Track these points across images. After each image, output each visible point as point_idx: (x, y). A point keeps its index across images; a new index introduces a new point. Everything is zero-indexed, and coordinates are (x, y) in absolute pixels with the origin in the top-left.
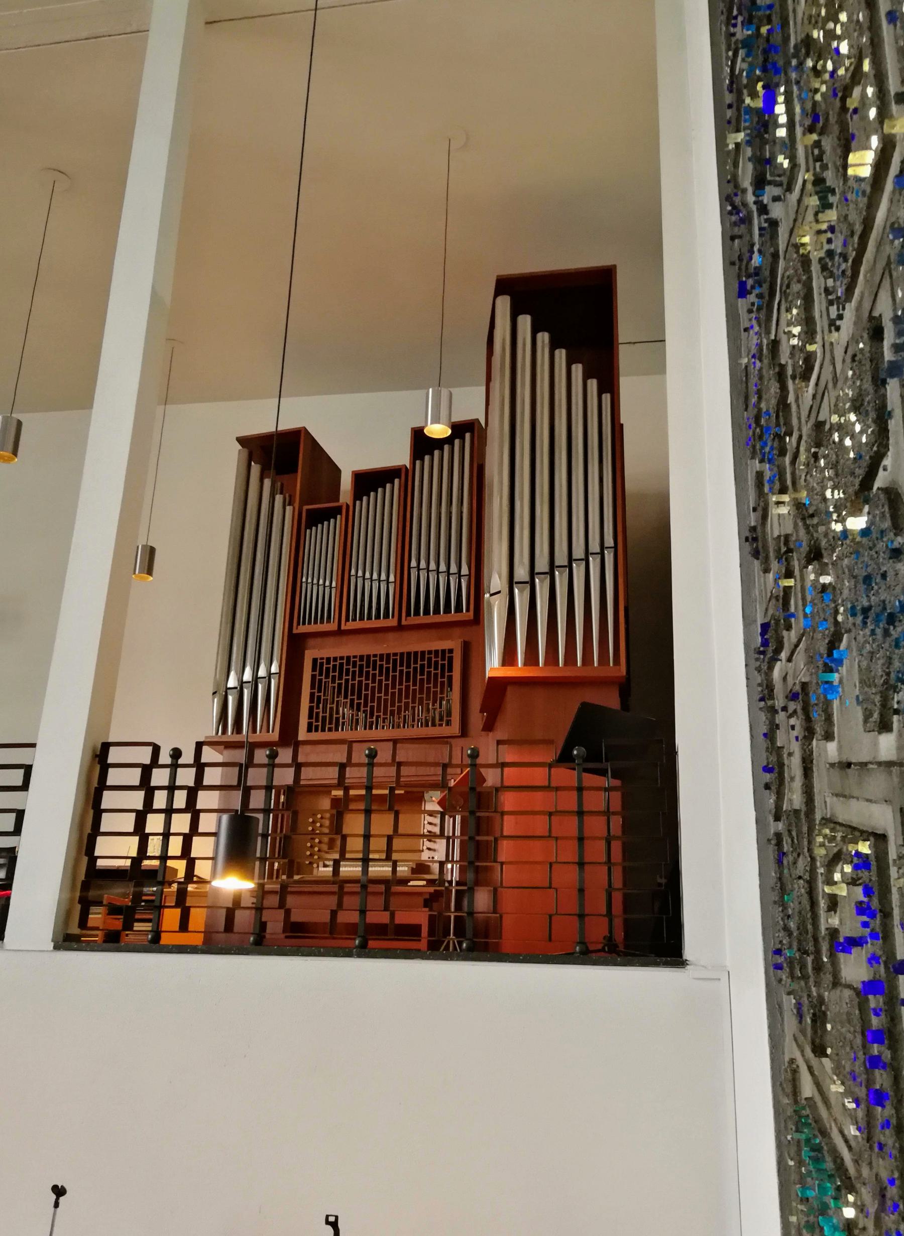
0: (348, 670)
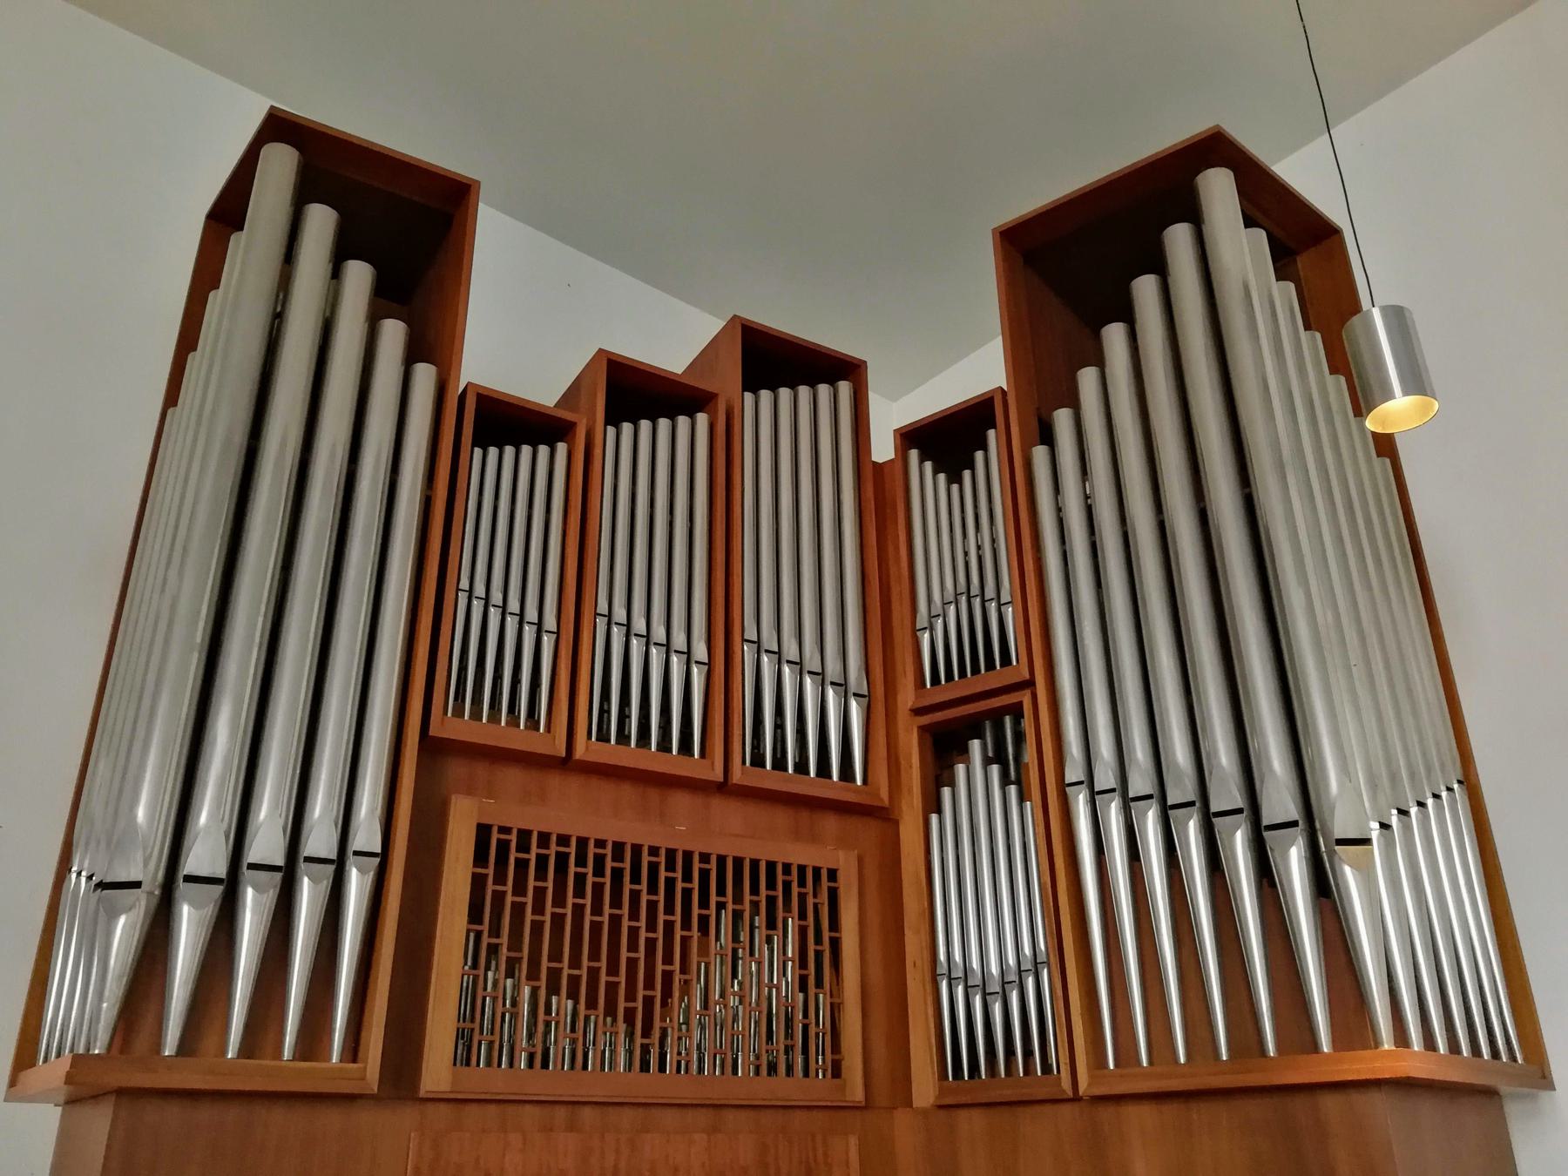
0: (580, 879)
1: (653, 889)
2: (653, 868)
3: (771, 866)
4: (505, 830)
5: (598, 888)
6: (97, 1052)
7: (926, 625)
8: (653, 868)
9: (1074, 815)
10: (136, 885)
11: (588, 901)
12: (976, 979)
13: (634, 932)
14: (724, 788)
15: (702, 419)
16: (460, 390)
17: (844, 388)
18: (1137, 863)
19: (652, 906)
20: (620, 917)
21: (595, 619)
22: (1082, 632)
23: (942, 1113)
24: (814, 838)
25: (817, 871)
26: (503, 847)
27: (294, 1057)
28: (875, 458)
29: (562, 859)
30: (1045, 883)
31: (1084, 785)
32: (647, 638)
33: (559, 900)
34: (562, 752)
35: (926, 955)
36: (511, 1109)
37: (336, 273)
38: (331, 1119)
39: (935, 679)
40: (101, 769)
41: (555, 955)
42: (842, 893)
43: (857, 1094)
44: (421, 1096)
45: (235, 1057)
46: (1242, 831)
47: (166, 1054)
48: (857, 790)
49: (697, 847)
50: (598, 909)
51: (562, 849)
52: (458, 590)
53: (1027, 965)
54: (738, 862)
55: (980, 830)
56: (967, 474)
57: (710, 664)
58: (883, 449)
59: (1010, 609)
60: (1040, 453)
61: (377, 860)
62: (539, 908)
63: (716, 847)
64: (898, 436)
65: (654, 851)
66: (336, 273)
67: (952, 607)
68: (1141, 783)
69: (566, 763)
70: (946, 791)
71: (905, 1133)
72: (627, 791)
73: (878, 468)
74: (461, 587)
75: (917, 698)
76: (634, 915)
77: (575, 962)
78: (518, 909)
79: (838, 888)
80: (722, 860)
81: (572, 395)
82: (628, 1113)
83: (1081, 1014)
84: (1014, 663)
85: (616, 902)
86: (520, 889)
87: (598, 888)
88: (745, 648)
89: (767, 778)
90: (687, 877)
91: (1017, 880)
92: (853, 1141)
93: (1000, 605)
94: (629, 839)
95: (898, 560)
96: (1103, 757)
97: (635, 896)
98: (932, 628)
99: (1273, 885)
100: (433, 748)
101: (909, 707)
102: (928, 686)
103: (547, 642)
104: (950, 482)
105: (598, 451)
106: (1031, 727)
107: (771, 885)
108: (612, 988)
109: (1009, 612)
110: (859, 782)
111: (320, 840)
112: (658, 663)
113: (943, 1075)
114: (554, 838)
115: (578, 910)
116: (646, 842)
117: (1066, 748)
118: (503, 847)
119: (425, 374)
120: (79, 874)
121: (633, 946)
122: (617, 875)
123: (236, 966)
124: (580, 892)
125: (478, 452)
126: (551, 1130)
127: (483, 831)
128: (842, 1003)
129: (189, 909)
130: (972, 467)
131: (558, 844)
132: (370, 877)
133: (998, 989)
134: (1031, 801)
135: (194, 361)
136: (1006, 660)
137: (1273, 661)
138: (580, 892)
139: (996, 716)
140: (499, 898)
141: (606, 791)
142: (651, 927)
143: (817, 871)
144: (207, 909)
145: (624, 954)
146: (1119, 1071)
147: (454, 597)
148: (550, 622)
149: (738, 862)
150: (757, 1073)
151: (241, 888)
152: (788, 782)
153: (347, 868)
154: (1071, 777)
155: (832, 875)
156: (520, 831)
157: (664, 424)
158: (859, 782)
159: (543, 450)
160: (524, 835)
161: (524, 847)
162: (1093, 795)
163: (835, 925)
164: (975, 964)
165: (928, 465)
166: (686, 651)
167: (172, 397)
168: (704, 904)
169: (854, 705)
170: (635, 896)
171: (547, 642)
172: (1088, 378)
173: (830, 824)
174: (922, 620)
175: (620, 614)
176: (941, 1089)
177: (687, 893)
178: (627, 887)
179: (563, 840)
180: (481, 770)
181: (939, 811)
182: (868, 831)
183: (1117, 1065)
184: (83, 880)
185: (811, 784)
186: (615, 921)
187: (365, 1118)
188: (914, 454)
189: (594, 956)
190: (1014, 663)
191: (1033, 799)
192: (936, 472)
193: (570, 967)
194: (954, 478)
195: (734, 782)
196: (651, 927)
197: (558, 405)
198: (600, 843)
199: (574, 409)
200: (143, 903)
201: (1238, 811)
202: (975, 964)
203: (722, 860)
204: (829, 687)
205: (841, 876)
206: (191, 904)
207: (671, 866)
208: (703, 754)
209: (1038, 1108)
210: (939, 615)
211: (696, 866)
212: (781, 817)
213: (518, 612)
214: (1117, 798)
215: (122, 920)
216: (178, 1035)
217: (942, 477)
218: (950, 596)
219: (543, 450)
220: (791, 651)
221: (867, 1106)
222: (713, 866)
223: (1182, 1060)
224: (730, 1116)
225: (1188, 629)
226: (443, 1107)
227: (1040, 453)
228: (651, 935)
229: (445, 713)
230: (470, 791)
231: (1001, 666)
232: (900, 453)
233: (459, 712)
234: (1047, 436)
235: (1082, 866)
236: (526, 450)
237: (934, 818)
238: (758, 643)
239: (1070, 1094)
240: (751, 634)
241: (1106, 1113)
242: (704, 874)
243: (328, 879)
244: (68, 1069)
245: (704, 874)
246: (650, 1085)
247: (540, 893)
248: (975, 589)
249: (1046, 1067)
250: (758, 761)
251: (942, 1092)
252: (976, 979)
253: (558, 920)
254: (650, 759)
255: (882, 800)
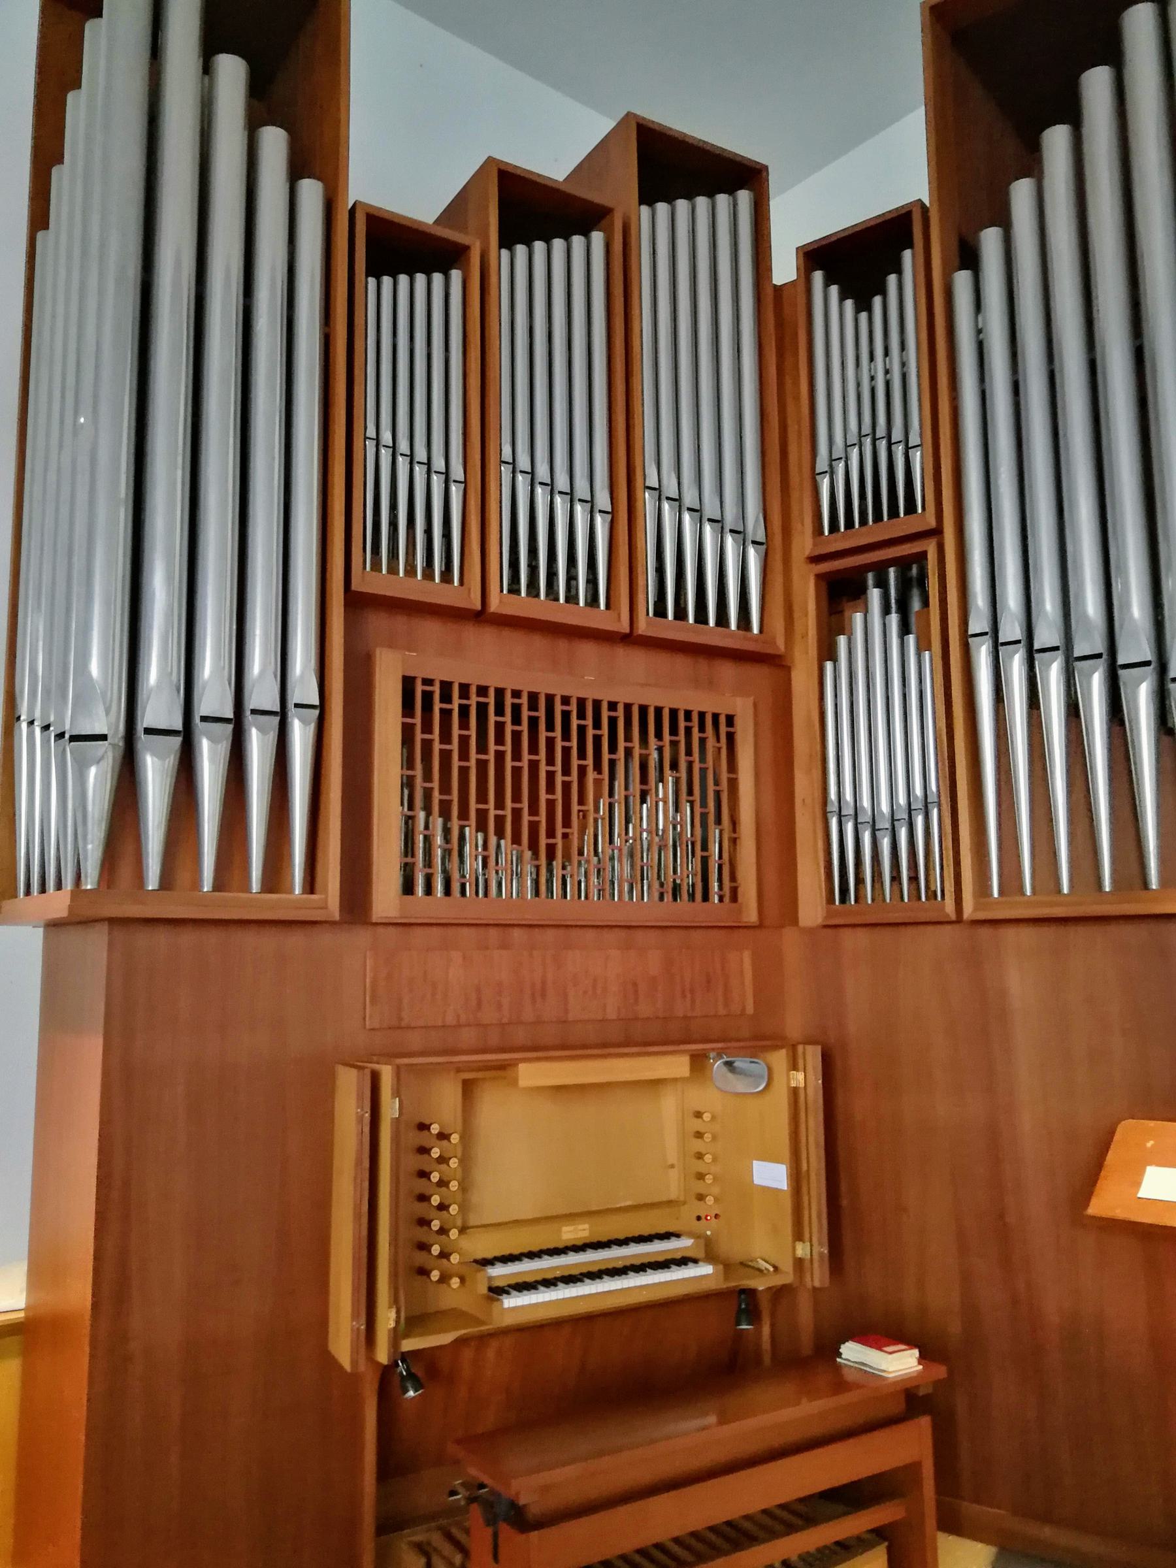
1: (566, 736)
2: (566, 715)
3: (674, 713)
4: (428, 682)
5: (516, 736)
6: (89, 887)
7: (827, 469)
8: (566, 715)
9: (975, 665)
10: (103, 737)
11: (508, 748)
12: (866, 817)
13: (551, 776)
14: (630, 639)
15: (597, 237)
16: (350, 206)
17: (744, 197)
18: (1035, 711)
19: (566, 751)
20: (431, 741)
21: (365, 442)
22: (996, 480)
23: (829, 931)
24: (711, 685)
25: (716, 717)
26: (428, 697)
27: (262, 889)
28: (775, 282)
29: (482, 709)
30: (940, 730)
31: (988, 636)
32: (551, 486)
33: (482, 748)
34: (627, 630)
35: (818, 794)
36: (451, 931)
37: (207, 69)
38: (295, 940)
39: (834, 527)
40: (34, 625)
41: (482, 797)
42: (739, 738)
43: (752, 916)
44: (374, 921)
45: (211, 890)
46: (1100, 674)
47: (150, 888)
48: (755, 639)
49: (606, 697)
50: (517, 756)
51: (482, 699)
52: (366, 438)
53: (918, 805)
54: (643, 709)
55: (858, 674)
56: (877, 301)
57: (613, 513)
58: (784, 270)
59: (918, 453)
60: (963, 279)
61: (317, 712)
62: (464, 755)
63: (622, 696)
64: (801, 254)
65: (566, 700)
66: (207, 69)
67: (856, 450)
68: (1047, 634)
69: (480, 616)
70: (842, 640)
71: (791, 944)
72: (539, 642)
73: (778, 289)
74: (368, 435)
75: (815, 545)
76: (550, 761)
77: (500, 805)
78: (446, 756)
79: (734, 733)
80: (628, 707)
81: (455, 211)
82: (550, 934)
83: (971, 849)
84: (920, 510)
85: (534, 749)
86: (446, 737)
87: (516, 736)
88: (502, 468)
89: (669, 629)
90: (597, 725)
91: (928, 728)
92: (747, 956)
93: (907, 449)
94: (543, 689)
95: (797, 398)
96: (1009, 609)
97: (550, 742)
98: (832, 472)
99: (1122, 723)
100: (356, 602)
101: (806, 556)
102: (826, 533)
103: (455, 491)
104: (858, 310)
105: (493, 279)
106: (934, 574)
107: (674, 731)
108: (534, 827)
109: (917, 457)
110: (756, 630)
111: (263, 694)
112: (563, 514)
113: (830, 899)
114: (473, 690)
115: (500, 756)
116: (559, 692)
117: (971, 599)
118: (428, 697)
119: (311, 191)
120: (31, 723)
121: (551, 788)
122: (533, 722)
123: (201, 810)
124: (500, 740)
125: (372, 281)
126: (487, 948)
127: (408, 683)
128: (739, 838)
129: (152, 760)
130: (883, 292)
131: (478, 695)
132: (312, 728)
133: (888, 825)
134: (929, 650)
135: (60, 177)
136: (911, 508)
137: (691, 406)
138: (500, 740)
139: (903, 564)
140: (427, 745)
141: (516, 642)
142: (566, 771)
143: (716, 717)
144: (168, 760)
145: (543, 796)
146: (1004, 899)
147: (363, 446)
148: (457, 472)
149: (643, 709)
150: (661, 898)
151: (196, 739)
152: (690, 630)
153: (290, 720)
154: (973, 628)
155: (730, 720)
156: (442, 683)
157: (558, 244)
158: (756, 630)
159: (437, 278)
160: (446, 687)
161: (446, 697)
162: (996, 646)
163: (732, 766)
164: (866, 802)
165: (834, 290)
166: (569, 492)
167: (39, 218)
168: (613, 749)
169: (752, 552)
170: (550, 742)
171: (455, 491)
172: (1022, 192)
173: (727, 671)
174: (822, 464)
175: (523, 462)
176: (828, 912)
177: (597, 740)
178: (543, 735)
179: (482, 691)
180: (400, 623)
181: (834, 658)
182: (759, 674)
183: (1001, 892)
184: (38, 731)
185: (709, 633)
186: (534, 765)
187: (325, 939)
188: (818, 277)
189: (517, 798)
190: (920, 510)
191: (933, 649)
192: (842, 298)
193: (496, 808)
194: (864, 305)
195: (640, 632)
196: (566, 771)
197: (438, 222)
198: (516, 694)
199: (463, 228)
200: (110, 755)
201: (1146, 664)
202: (866, 802)
203: (628, 707)
204: (729, 534)
205: (738, 722)
206: (153, 754)
207: (581, 715)
208: (608, 606)
209: (921, 928)
210: (841, 458)
211: (605, 714)
212: (681, 664)
213: (425, 461)
214: (1021, 650)
215: (93, 771)
216: (158, 872)
217: (849, 304)
218: (853, 438)
219: (437, 278)
220: (690, 499)
221: (760, 926)
222: (620, 713)
223: (1066, 890)
224: (639, 935)
225: (1068, 471)
226: (391, 930)
227: (963, 279)
228: (566, 779)
229: (365, 568)
230: (391, 645)
231: (905, 514)
232: (803, 275)
233: (376, 566)
234: (969, 258)
235: (980, 715)
236: (420, 278)
237: (829, 665)
238: (659, 490)
239: (953, 917)
240: (653, 481)
241: (985, 932)
242: (613, 722)
243: (274, 731)
244: (69, 903)
245: (613, 722)
246: (555, 907)
247: (464, 740)
248: (881, 431)
249: (931, 895)
250: (660, 611)
251: (829, 914)
252: (866, 817)
253: (482, 766)
254: (559, 612)
255: (778, 648)
